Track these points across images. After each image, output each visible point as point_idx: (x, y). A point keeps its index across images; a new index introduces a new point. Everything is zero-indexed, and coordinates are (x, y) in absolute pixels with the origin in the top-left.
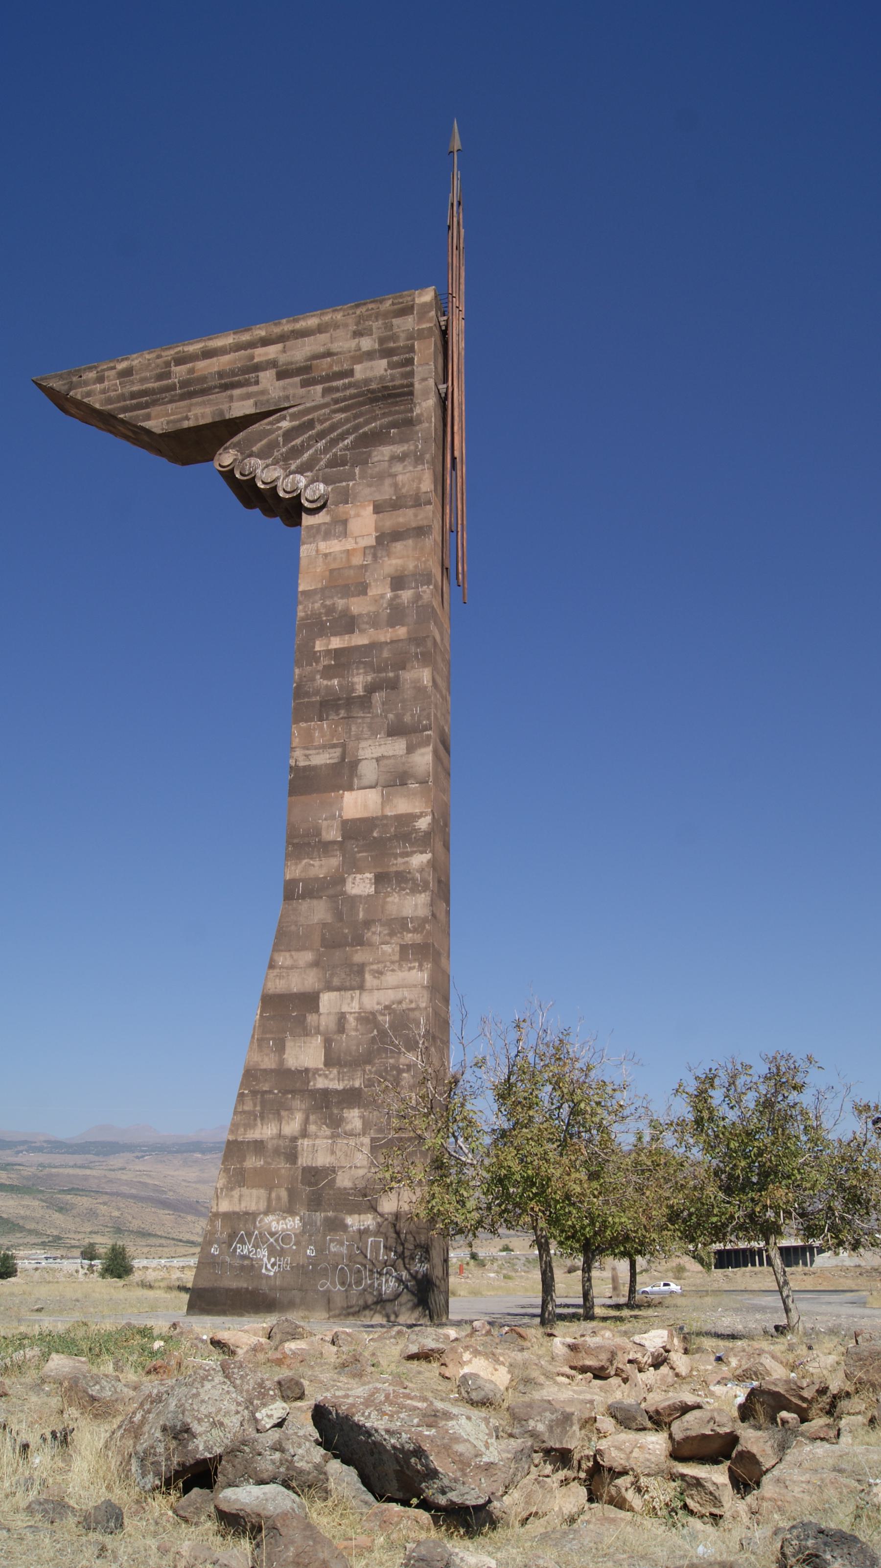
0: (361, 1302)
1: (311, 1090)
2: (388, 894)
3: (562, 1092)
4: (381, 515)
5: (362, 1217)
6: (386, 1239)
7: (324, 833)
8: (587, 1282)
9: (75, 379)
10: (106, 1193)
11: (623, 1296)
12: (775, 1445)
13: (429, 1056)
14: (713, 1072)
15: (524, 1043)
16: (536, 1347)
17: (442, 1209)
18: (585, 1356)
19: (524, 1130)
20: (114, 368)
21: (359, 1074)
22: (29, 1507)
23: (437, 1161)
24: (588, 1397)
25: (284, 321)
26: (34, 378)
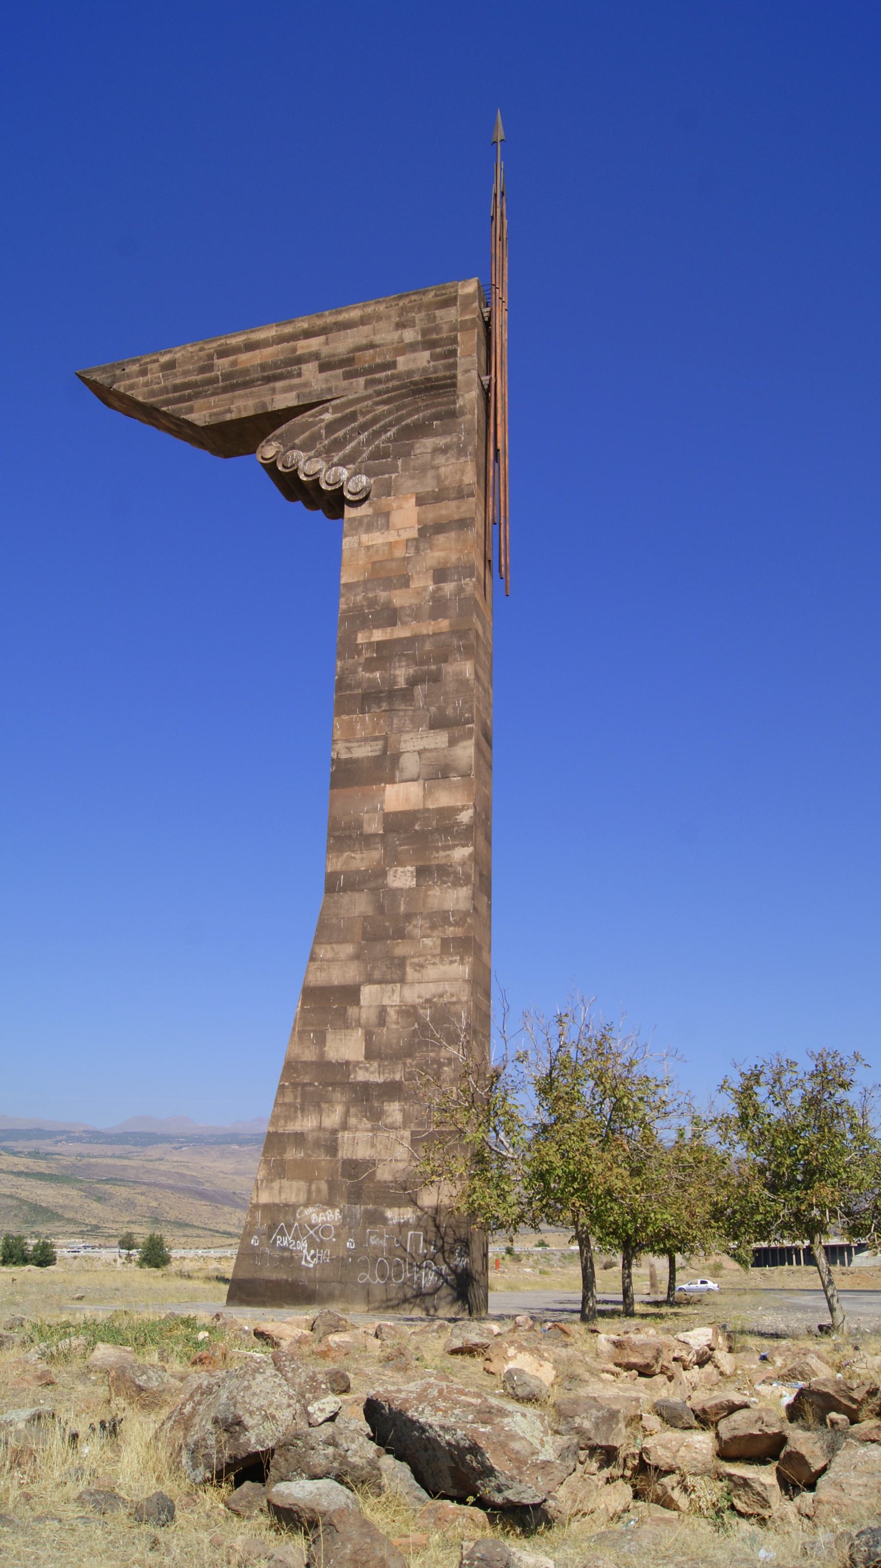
0: (400, 1295)
1: (351, 1083)
2: (429, 888)
3: (605, 1087)
4: (423, 507)
5: (402, 1210)
6: (426, 1232)
7: (365, 826)
8: (627, 1277)
9: (118, 372)
10: (144, 1184)
11: (661, 1293)
12: (825, 1447)
13: (470, 1050)
14: (758, 1068)
15: (566, 1038)
16: (580, 1343)
17: (482, 1203)
18: (630, 1353)
19: (566, 1125)
20: (157, 361)
21: (400, 1067)
22: (80, 1497)
23: (478, 1155)
24: (634, 1394)
25: (327, 313)
26: (77, 372)
